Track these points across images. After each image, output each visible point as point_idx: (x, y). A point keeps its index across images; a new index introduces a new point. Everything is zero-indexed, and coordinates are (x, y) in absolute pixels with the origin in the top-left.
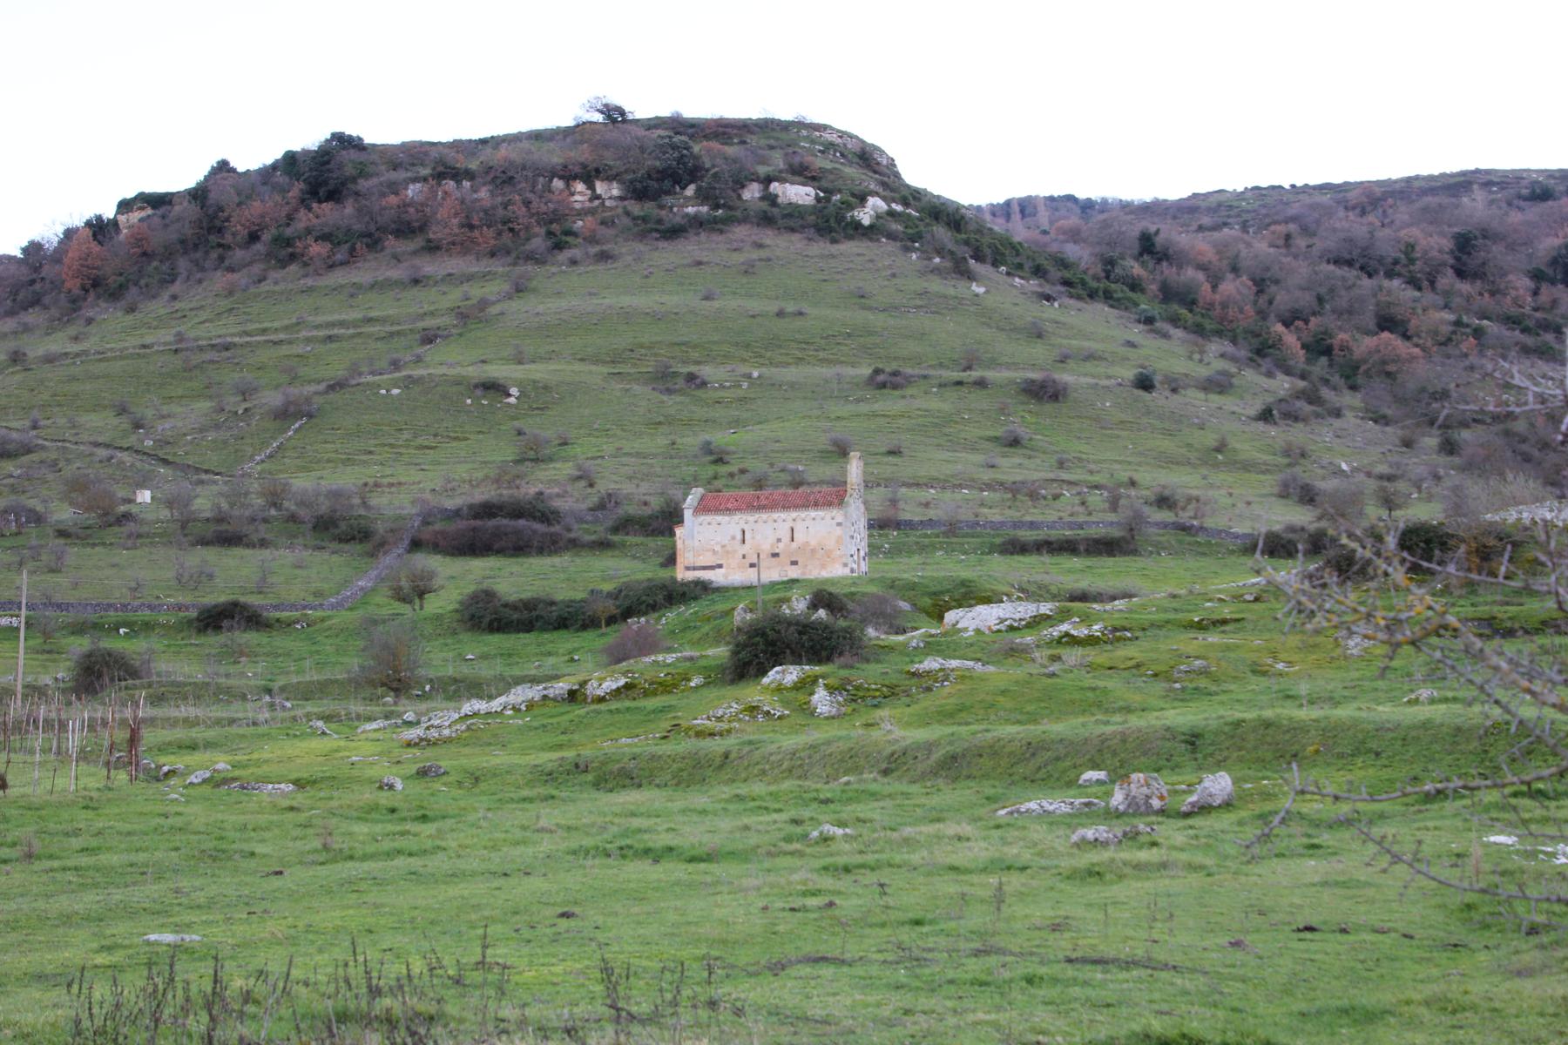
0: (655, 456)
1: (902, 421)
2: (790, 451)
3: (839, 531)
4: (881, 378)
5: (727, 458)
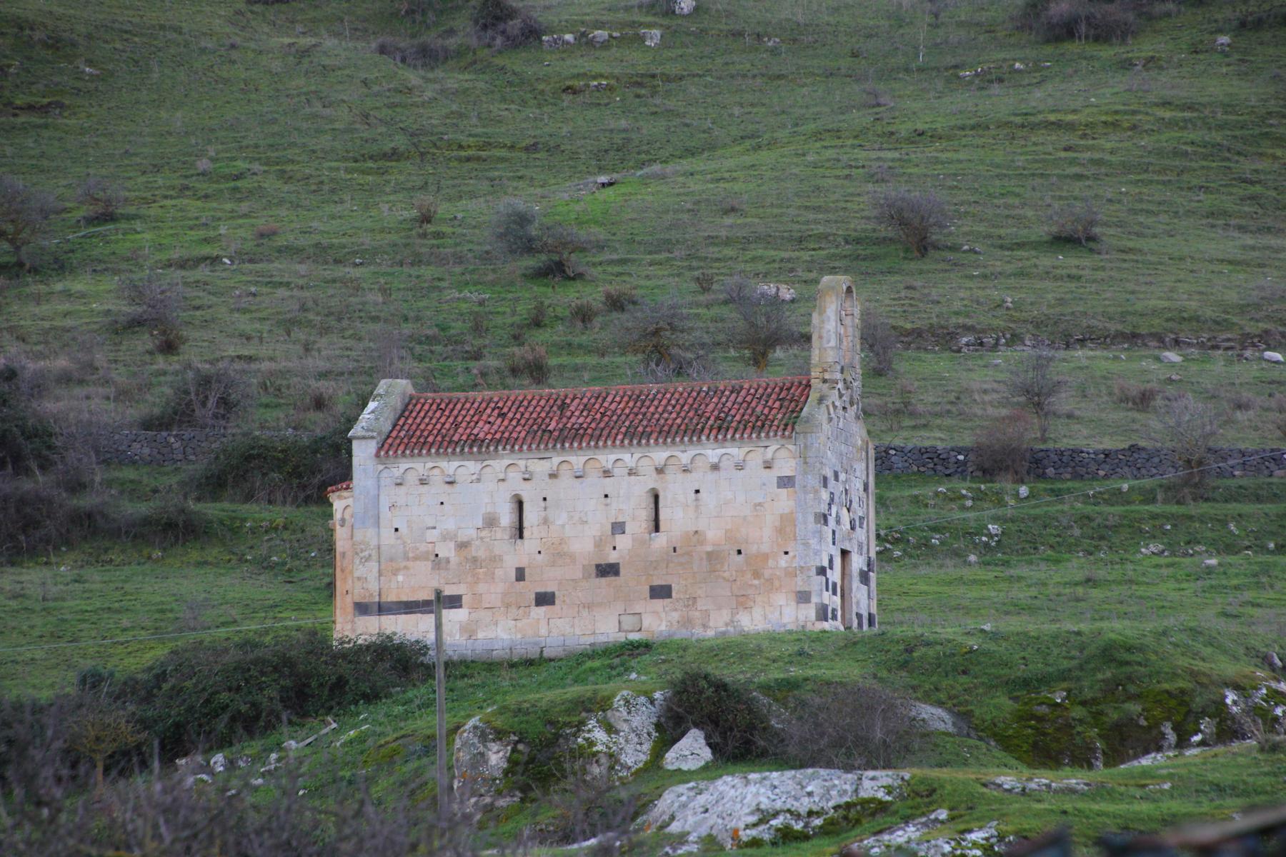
0: (367, 256)
2: (766, 240)
3: (784, 501)
5: (576, 261)
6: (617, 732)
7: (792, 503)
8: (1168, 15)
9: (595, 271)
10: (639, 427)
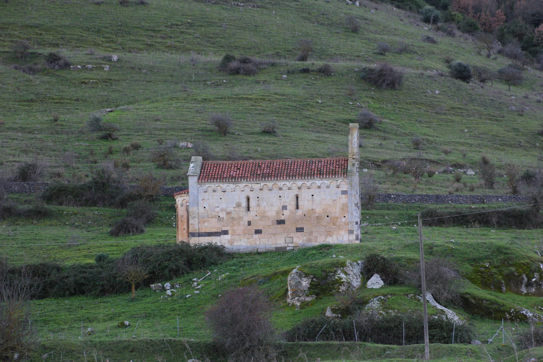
0: (41, 131)
1: (264, 104)
2: (173, 129)
3: (344, 199)
4: (234, 64)
5: (115, 134)
6: (349, 275)
7: (346, 200)
8: (265, 68)
9: (121, 137)
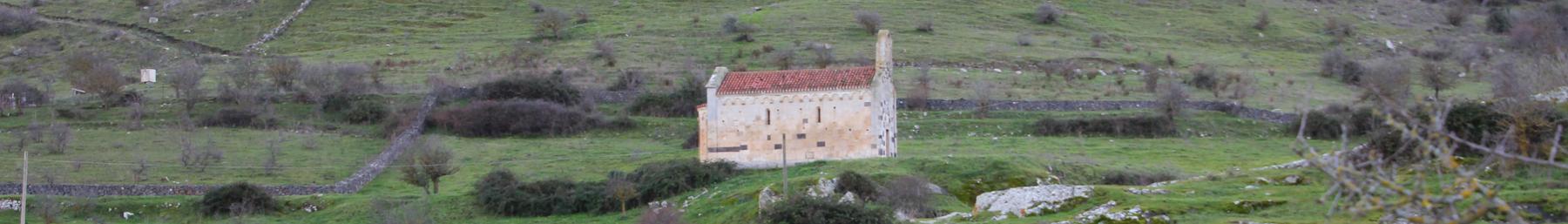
0: (677, 33)
5: (751, 36)
10: (813, 85)
